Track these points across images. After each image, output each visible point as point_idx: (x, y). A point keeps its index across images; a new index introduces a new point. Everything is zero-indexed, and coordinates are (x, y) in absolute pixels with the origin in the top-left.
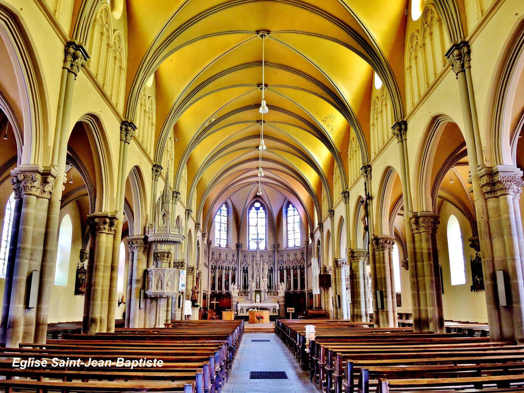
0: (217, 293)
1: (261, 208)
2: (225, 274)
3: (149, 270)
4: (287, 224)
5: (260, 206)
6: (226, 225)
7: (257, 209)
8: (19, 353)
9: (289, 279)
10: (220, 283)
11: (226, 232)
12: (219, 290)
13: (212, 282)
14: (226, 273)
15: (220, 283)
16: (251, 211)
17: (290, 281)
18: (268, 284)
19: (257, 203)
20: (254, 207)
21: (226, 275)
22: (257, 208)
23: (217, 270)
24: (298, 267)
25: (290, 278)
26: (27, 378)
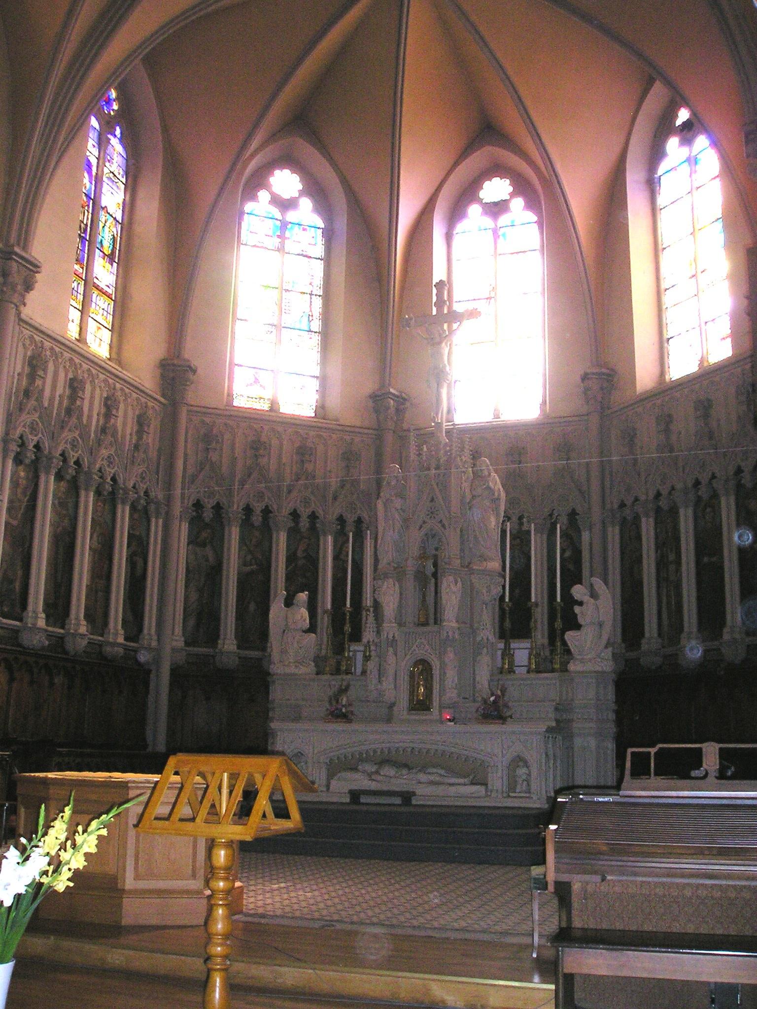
0: (232, 662)
1: (518, 203)
2: (291, 558)
3: (514, 644)
4: (657, 250)
5: (512, 195)
6: (318, 303)
7: (497, 209)
8: (601, 799)
9: (672, 568)
10: (252, 607)
11: (317, 338)
12: (243, 640)
13: (194, 596)
14: (300, 554)
15: (252, 607)
16: (460, 227)
17: (678, 586)
18: (502, 598)
19: (496, 181)
20: (480, 201)
21: (301, 562)
22: (496, 204)
23: (234, 534)
24: (718, 485)
25: (678, 562)
26: (49, 938)
